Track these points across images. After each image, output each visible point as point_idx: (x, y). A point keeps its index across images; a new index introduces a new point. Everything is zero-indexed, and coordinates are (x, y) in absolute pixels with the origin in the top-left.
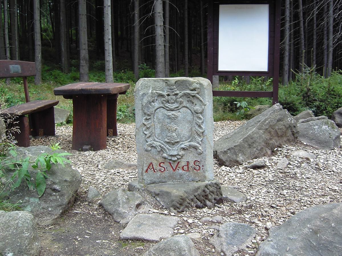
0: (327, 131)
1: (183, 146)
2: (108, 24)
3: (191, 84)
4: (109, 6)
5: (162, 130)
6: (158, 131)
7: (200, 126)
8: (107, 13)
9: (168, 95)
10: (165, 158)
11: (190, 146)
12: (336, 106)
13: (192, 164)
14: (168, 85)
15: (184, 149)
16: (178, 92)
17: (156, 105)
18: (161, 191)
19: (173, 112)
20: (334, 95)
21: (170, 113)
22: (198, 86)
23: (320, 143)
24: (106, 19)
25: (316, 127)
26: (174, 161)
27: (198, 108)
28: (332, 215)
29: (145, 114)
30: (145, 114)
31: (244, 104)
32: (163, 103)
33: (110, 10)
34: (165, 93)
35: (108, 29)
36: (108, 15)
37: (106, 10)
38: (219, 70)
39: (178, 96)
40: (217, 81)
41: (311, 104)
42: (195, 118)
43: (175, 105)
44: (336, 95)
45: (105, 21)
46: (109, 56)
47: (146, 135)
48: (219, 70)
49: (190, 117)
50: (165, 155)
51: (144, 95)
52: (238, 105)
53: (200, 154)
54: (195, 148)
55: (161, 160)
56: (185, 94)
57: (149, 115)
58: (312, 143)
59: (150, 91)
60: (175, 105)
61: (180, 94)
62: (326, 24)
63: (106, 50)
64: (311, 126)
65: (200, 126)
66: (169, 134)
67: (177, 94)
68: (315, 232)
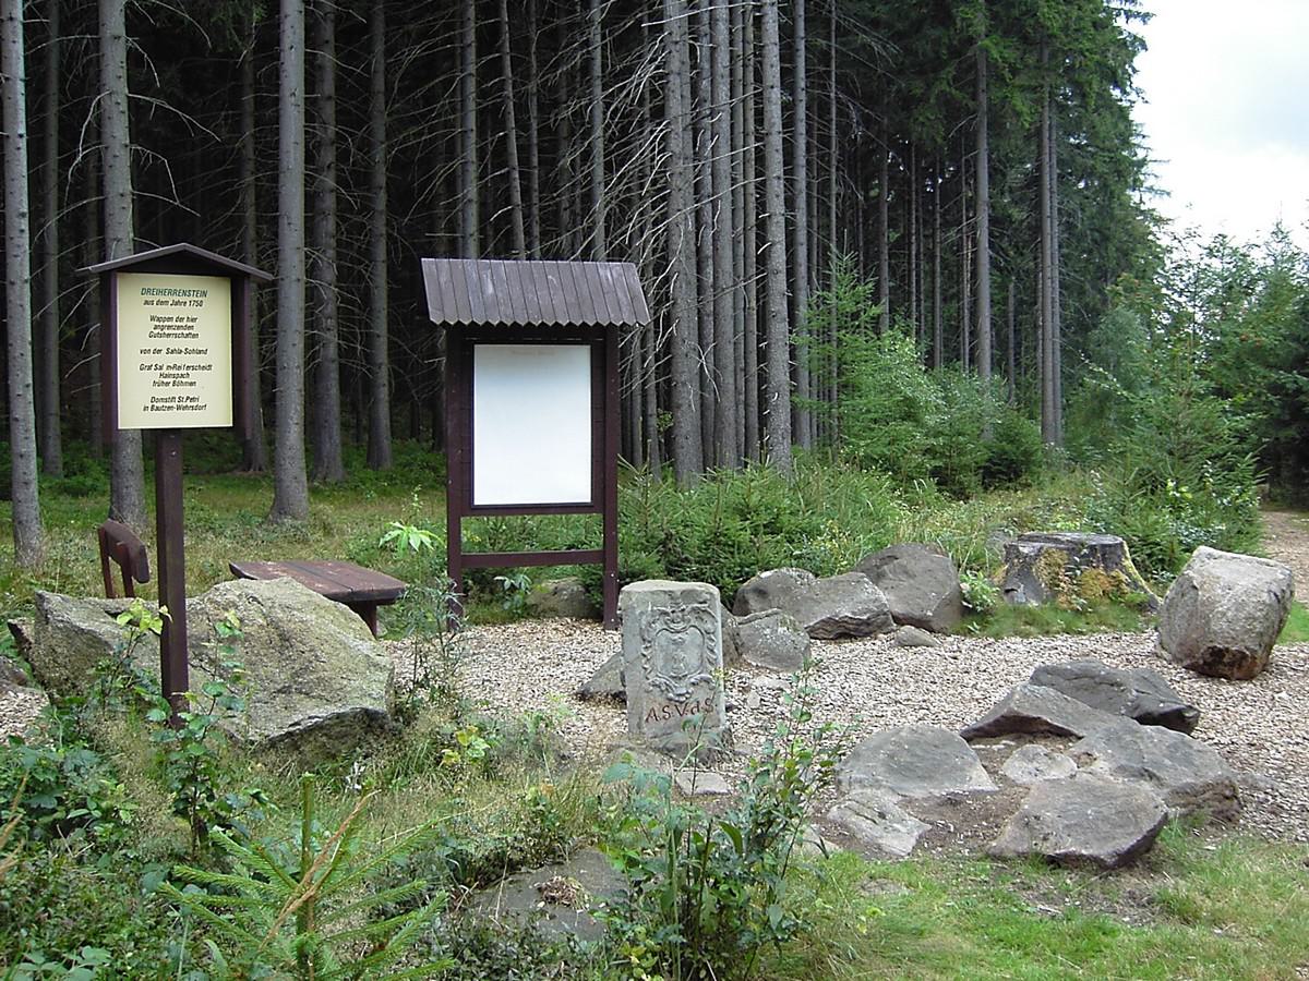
0: (788, 637)
1: (693, 680)
2: (23, 339)
3: (699, 594)
4: (26, 281)
5: (666, 661)
6: (660, 663)
7: (712, 651)
8: (18, 302)
9: (673, 612)
10: (670, 700)
11: (702, 679)
12: (739, 572)
13: (702, 704)
14: (672, 598)
15: (693, 684)
16: (684, 607)
17: (658, 626)
18: (676, 745)
19: (679, 635)
20: (726, 544)
21: (676, 637)
22: (708, 596)
23: (779, 661)
24: (17, 323)
25: (768, 631)
26: (681, 703)
27: (709, 626)
28: (902, 737)
29: (644, 640)
30: (644, 640)
31: (522, 579)
32: (666, 623)
33: (29, 294)
34: (669, 610)
35: (22, 355)
36: (24, 310)
37: (18, 293)
38: (477, 502)
39: (686, 613)
40: (303, 492)
41: (679, 572)
42: (706, 640)
43: (682, 625)
44: (733, 546)
45: (11, 329)
46: (26, 438)
47: (645, 669)
48: (477, 502)
49: (699, 640)
50: (671, 695)
51: (642, 613)
52: (507, 583)
53: (712, 689)
54: (707, 681)
55: (665, 703)
56: (693, 609)
57: (649, 642)
58: (764, 661)
59: (650, 609)
60: (682, 625)
61: (688, 609)
62: (637, 341)
63: (17, 420)
64: (757, 629)
65: (712, 651)
66: (675, 666)
67: (683, 610)
68: (891, 757)
